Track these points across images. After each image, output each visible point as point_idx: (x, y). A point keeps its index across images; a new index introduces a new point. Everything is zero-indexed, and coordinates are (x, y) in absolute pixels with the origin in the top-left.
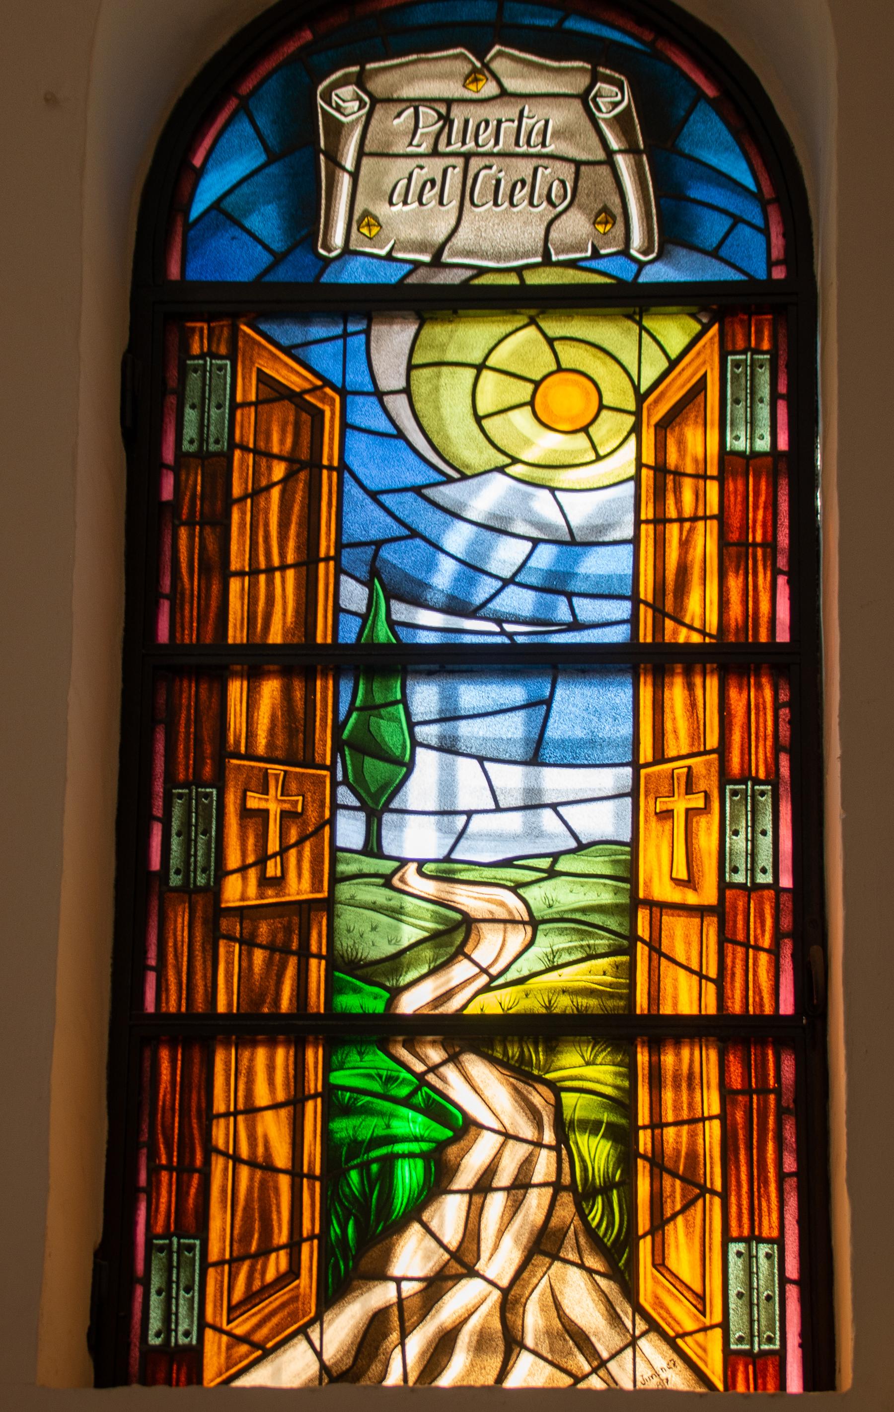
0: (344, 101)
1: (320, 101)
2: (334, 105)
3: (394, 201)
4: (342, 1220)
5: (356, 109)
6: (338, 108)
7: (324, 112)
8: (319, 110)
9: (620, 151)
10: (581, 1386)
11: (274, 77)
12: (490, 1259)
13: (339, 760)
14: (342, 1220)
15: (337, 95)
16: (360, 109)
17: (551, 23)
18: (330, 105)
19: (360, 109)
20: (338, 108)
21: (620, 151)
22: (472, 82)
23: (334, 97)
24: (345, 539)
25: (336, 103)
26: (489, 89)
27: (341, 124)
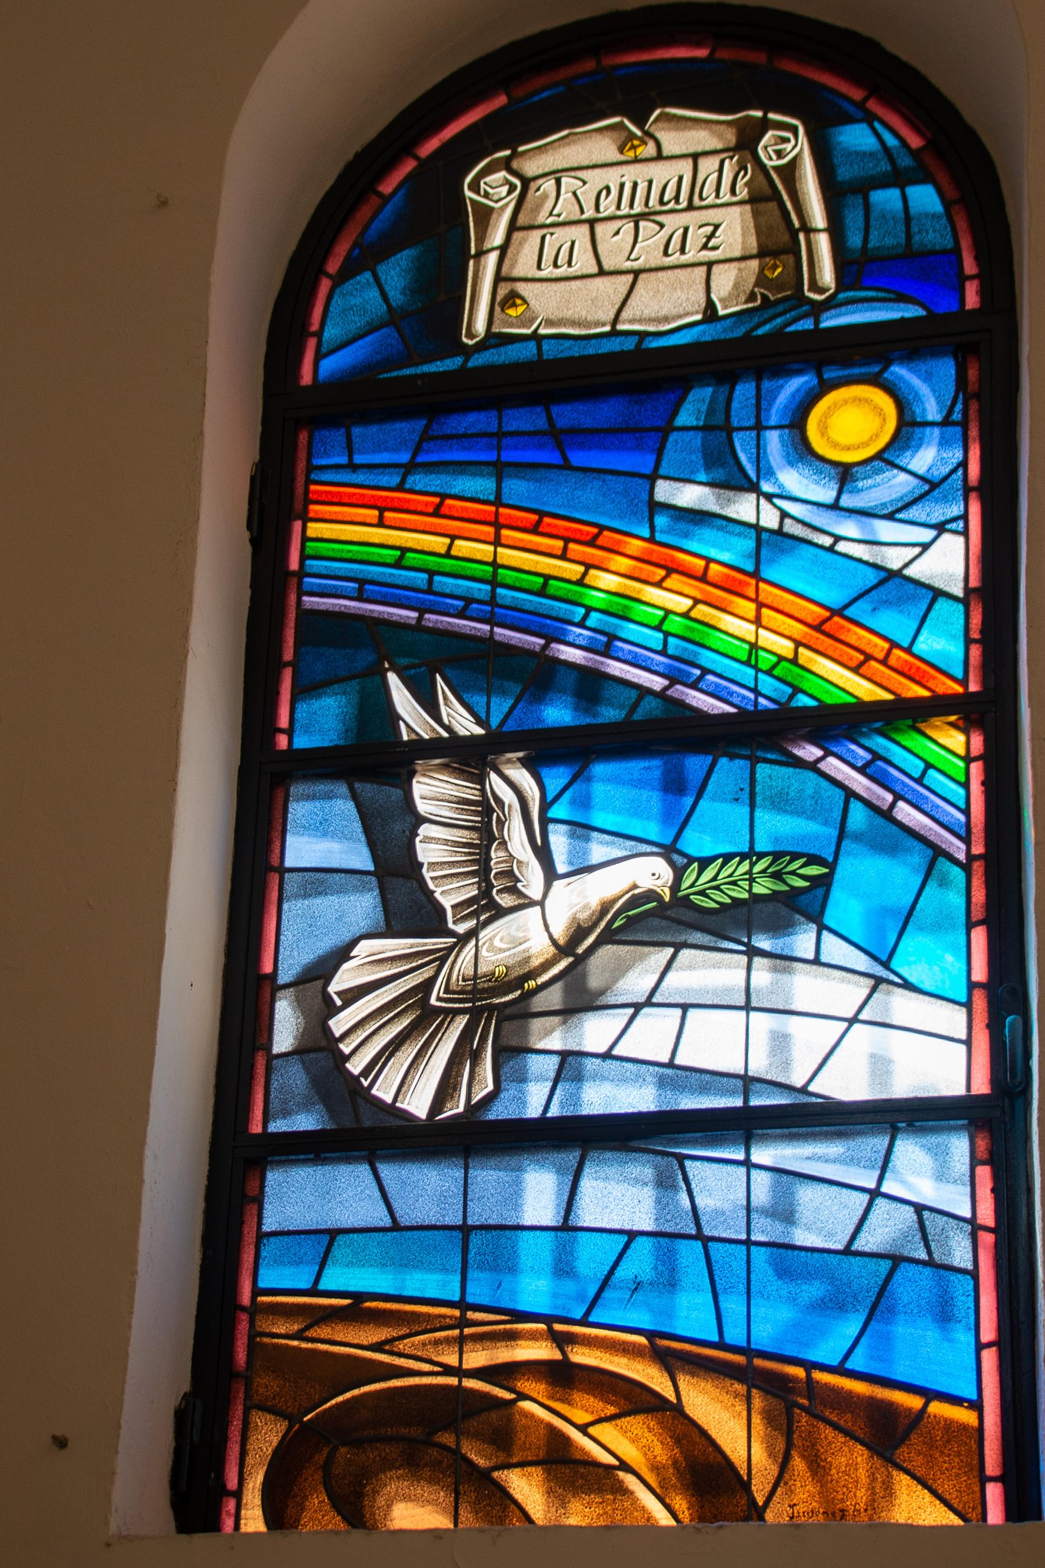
0: (492, 188)
1: (468, 193)
2: (482, 193)
3: (559, 263)
4: (784, 759)
5: (504, 194)
6: (487, 195)
7: (471, 200)
8: (468, 201)
9: (819, 231)
10: (621, 1474)
11: (461, 1512)
12: (808, 1158)
13: (503, 1317)
14: (784, 759)
15: (485, 183)
16: (509, 193)
17: (481, 1462)
18: (478, 193)
19: (509, 193)
20: (487, 195)
21: (819, 231)
22: (629, 149)
23: (482, 185)
24: (595, 270)
25: (485, 191)
26: (650, 150)
27: (491, 210)
